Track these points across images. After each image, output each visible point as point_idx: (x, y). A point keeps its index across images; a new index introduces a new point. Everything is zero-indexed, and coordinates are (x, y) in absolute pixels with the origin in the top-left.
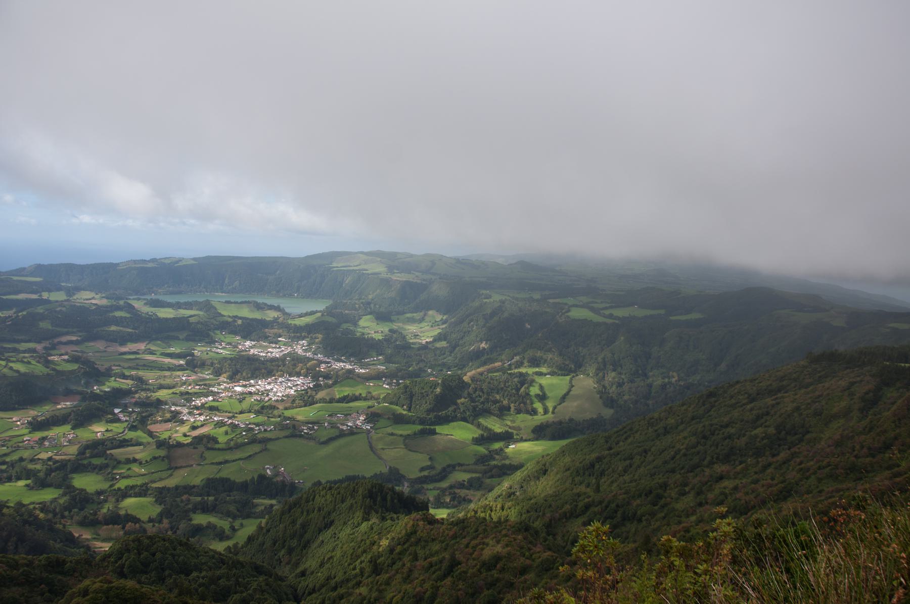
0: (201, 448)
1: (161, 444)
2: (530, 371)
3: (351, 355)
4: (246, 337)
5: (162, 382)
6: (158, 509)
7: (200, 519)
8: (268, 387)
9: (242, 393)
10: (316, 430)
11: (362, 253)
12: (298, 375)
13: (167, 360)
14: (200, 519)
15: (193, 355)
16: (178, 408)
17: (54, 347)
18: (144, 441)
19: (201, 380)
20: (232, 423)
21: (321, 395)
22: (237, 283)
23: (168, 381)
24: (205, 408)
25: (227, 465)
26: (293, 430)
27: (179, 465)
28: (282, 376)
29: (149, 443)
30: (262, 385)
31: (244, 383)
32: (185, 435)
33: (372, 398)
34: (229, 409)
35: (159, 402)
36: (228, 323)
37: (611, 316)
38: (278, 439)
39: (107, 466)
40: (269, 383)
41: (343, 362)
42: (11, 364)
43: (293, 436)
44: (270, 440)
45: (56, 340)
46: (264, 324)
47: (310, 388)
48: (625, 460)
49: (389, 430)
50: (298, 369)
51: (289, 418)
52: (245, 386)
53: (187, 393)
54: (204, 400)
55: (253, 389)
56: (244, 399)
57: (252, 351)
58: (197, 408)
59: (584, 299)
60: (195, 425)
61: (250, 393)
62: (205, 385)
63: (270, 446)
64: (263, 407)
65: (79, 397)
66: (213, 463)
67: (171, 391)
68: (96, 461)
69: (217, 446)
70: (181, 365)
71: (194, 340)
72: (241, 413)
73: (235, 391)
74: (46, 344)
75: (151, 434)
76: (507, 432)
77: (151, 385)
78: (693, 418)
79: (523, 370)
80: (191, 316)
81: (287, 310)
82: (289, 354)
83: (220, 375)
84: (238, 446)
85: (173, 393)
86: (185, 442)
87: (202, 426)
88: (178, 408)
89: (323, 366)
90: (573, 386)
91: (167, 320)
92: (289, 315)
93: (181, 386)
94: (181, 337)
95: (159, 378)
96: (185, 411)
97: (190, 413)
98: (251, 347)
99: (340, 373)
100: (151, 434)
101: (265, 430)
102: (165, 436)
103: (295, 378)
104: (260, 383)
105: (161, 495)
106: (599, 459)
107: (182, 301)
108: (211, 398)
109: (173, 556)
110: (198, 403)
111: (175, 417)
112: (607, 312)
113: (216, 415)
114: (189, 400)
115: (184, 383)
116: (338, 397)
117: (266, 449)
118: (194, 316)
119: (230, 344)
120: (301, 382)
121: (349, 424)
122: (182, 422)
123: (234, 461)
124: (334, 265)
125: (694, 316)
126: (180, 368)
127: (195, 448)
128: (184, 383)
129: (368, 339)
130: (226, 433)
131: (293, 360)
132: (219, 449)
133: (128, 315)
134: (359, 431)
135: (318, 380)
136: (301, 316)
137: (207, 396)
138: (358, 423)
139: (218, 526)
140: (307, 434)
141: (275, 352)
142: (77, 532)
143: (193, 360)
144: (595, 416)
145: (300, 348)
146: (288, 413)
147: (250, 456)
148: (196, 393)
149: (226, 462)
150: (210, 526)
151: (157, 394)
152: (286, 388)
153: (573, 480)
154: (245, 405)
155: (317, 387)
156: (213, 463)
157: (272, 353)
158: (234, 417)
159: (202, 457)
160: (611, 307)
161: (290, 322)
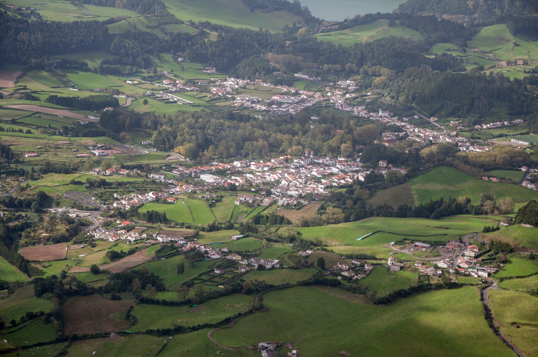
0: (128, 300)
1: (45, 287)
3: (453, 114)
4: (228, 69)
5: (51, 158)
8: (271, 177)
9: (216, 188)
10: (368, 274)
12: (335, 152)
13: (62, 113)
15: (115, 103)
16: (83, 214)
18: (11, 279)
19: (131, 158)
20: (193, 249)
21: (381, 198)
24: (138, 215)
25: (180, 337)
26: (322, 275)
27: (80, 333)
28: (300, 155)
29: (19, 284)
30: (258, 171)
31: (221, 166)
33: (495, 209)
34: (188, 221)
35: (44, 201)
36: (188, 38)
40: (273, 169)
41: (433, 128)
43: (318, 282)
44: (270, 288)
46: (263, 42)
50: (333, 142)
51: (311, 244)
52: (221, 173)
53: (103, 183)
54: (136, 199)
55: (239, 181)
56: (219, 200)
57: (239, 100)
58: (122, 215)
60: (118, 249)
61: (233, 188)
62: (140, 167)
63: (269, 301)
64: (258, 220)
66: (150, 332)
67: (69, 178)
69: (160, 296)
70: (91, 124)
71: (117, 73)
72: (213, 228)
73: (202, 183)
75: (24, 266)
77: (29, 163)
80: (111, 21)
81: (315, 14)
82: (316, 109)
83: (171, 148)
84: (203, 300)
85: (74, 182)
86: (97, 286)
87: (132, 252)
88: (83, 214)
89: (388, 136)
90: (240, 314)
91: (59, 26)
92: (319, 22)
93: (91, 168)
94: (91, 64)
95: (45, 149)
96: (98, 219)
97: (107, 225)
99: (425, 152)
100: (24, 266)
101: (261, 268)
102: (54, 270)
103: (327, 160)
104: (253, 167)
108: (151, 195)
110: (125, 204)
111: (76, 231)
113: (161, 232)
114: (105, 199)
115: (98, 163)
116: (417, 204)
117: (261, 308)
119: (192, 82)
120: (344, 172)
121: (441, 264)
122: (92, 243)
123: (194, 329)
126: (89, 130)
127: (114, 298)
128: (98, 163)
129: (491, 80)
130: (181, 270)
131: (323, 121)
132: (165, 303)
134: (461, 280)
135: (376, 166)
136: (343, 26)
137: (143, 191)
138: (461, 262)
140: (349, 279)
143: (115, 115)
145: (339, 95)
146: (308, 234)
147: (228, 321)
148: (120, 184)
149: (179, 330)
151: (40, 183)
152: (307, 179)
154: (221, 214)
155: (373, 182)
156: (150, 332)
157: (280, 104)
158: (197, 235)
159: (128, 317)
161: (320, 37)
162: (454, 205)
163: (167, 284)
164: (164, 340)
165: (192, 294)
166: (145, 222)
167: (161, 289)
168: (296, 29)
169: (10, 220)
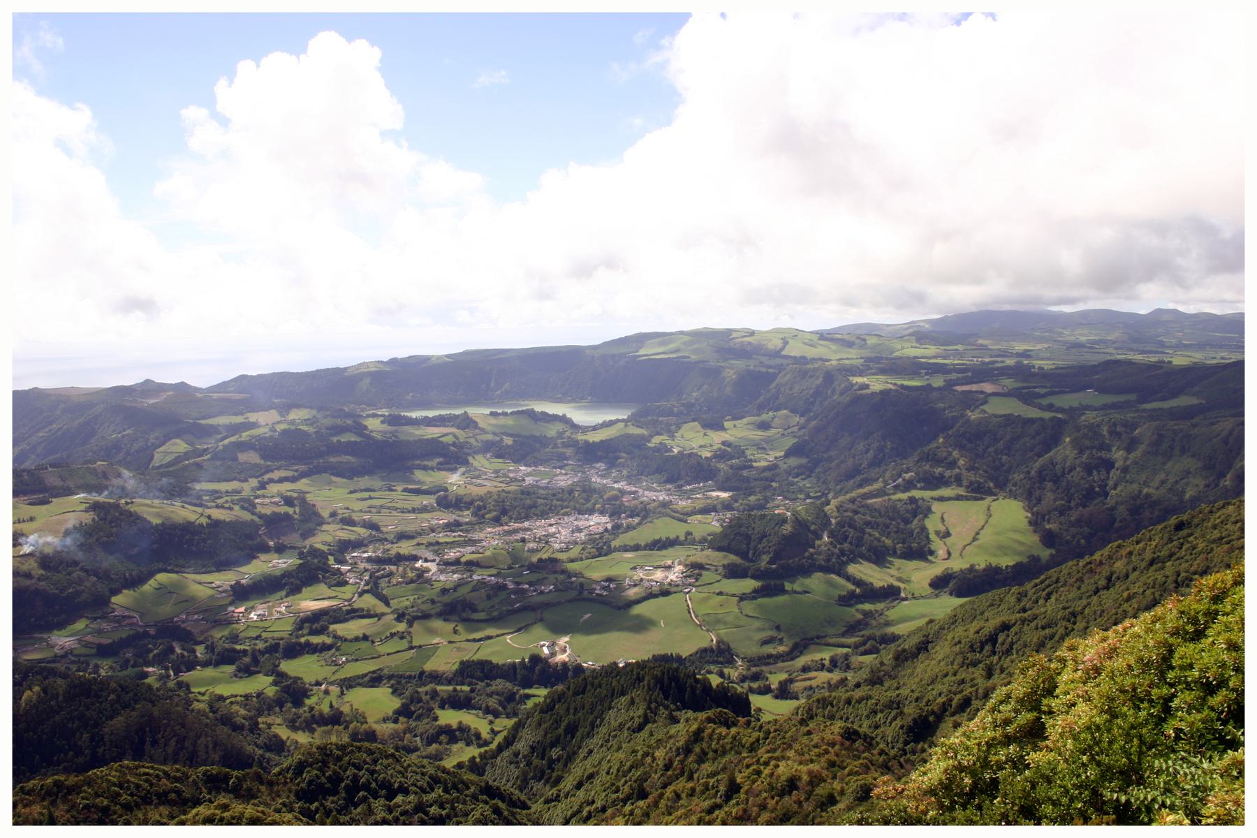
2: (927, 494)
6: (396, 703)
7: (449, 717)
8: (552, 530)
11: (682, 333)
14: (449, 717)
15: (446, 490)
17: (263, 486)
22: (507, 386)
23: (411, 528)
32: (433, 602)
37: (1050, 407)
38: (559, 603)
39: (329, 647)
42: (208, 512)
45: (266, 477)
47: (606, 530)
48: (1043, 628)
49: (717, 588)
53: (438, 543)
59: (1009, 383)
65: (296, 552)
67: (414, 542)
68: (316, 640)
69: (476, 616)
74: (254, 482)
76: (891, 587)
78: (1152, 563)
79: (916, 493)
96: (433, 567)
98: (528, 474)
101: (542, 592)
105: (397, 682)
106: (1005, 627)
107: (550, 412)
109: (372, 772)
112: (1045, 402)
118: (446, 435)
124: (641, 352)
125: (1183, 401)
133: (358, 439)
139: (473, 726)
141: (564, 480)
142: (284, 733)
143: (446, 497)
144: (1025, 560)
150: (463, 729)
153: (965, 658)
160: (1052, 393)
161: (581, 437)
162: (314, 750)
163: (479, 608)
164: (477, 645)
165: (495, 614)
166: (1074, 562)
167: (475, 611)
168: (564, 432)
169: (378, 571)
